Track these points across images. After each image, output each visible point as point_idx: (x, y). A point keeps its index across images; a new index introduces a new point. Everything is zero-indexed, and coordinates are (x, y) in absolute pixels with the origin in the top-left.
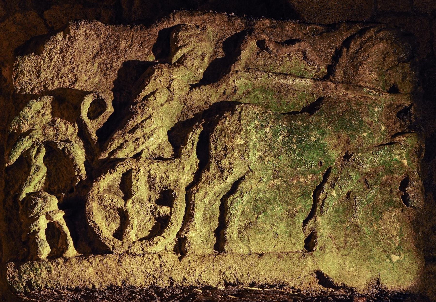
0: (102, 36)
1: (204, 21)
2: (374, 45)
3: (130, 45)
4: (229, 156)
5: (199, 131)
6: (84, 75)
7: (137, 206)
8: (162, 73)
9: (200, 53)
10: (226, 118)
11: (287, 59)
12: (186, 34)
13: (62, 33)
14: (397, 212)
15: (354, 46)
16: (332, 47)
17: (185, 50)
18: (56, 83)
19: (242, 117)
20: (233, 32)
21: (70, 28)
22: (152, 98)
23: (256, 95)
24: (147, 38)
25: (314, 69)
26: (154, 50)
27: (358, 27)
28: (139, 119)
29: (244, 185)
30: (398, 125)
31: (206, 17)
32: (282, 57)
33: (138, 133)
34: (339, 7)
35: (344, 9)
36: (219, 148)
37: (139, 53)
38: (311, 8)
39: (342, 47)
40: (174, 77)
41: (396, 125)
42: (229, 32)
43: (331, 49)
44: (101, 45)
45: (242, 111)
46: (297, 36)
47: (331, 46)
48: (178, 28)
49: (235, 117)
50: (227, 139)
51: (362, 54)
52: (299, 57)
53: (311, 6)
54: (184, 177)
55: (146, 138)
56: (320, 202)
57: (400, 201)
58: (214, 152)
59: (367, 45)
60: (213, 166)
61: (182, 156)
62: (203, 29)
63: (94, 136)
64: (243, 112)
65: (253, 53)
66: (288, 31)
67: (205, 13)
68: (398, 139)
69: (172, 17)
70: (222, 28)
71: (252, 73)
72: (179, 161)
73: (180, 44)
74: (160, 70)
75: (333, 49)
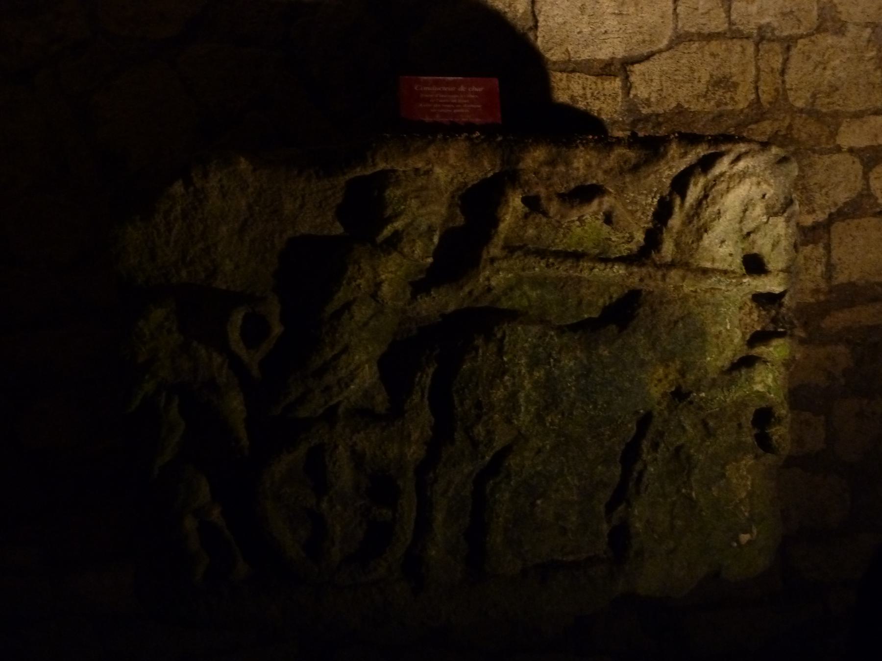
0: (251, 190)
1: (428, 162)
2: (728, 190)
3: (302, 206)
4: (485, 418)
5: (431, 371)
6: (227, 261)
7: (339, 508)
8: (361, 272)
9: (424, 227)
10: (476, 349)
11: (578, 223)
12: (399, 192)
13: (180, 182)
14: (748, 460)
15: (694, 192)
16: (653, 195)
17: (398, 224)
18: (184, 273)
19: (506, 348)
20: (481, 176)
21: (193, 174)
22: (346, 316)
23: (525, 293)
24: (329, 193)
25: (623, 237)
26: (341, 213)
27: (702, 151)
28: (329, 354)
29: (513, 462)
30: (755, 316)
31: (431, 151)
32: (568, 222)
33: (329, 379)
34: (621, 29)
35: (628, 31)
36: (468, 403)
37: (318, 221)
38: (579, 33)
39: (670, 194)
40: (383, 277)
41: (752, 317)
42: (474, 175)
43: (653, 198)
44: (250, 207)
45: (503, 337)
46: (593, 178)
47: (651, 191)
48: (385, 179)
49: (493, 347)
50: (480, 388)
51: (710, 210)
52: (598, 219)
53: (578, 30)
54: (412, 451)
55: (343, 386)
56: (635, 474)
57: (754, 443)
58: (459, 409)
59: (717, 191)
60: (459, 436)
61: (406, 415)
62: (428, 173)
63: (255, 372)
64: (507, 339)
65: (517, 216)
66: (578, 169)
67: (429, 143)
68: (760, 350)
69: (370, 160)
70: (462, 171)
71: (518, 261)
72: (400, 423)
73: (389, 212)
74: (357, 267)
75: (655, 197)
